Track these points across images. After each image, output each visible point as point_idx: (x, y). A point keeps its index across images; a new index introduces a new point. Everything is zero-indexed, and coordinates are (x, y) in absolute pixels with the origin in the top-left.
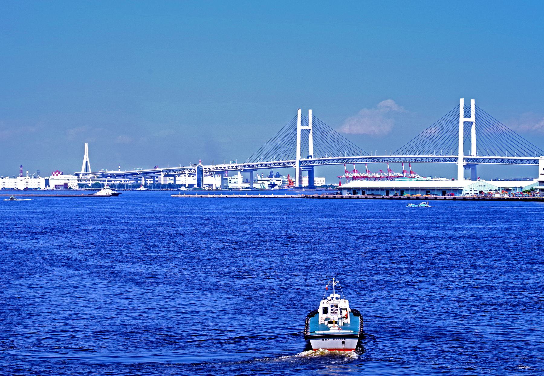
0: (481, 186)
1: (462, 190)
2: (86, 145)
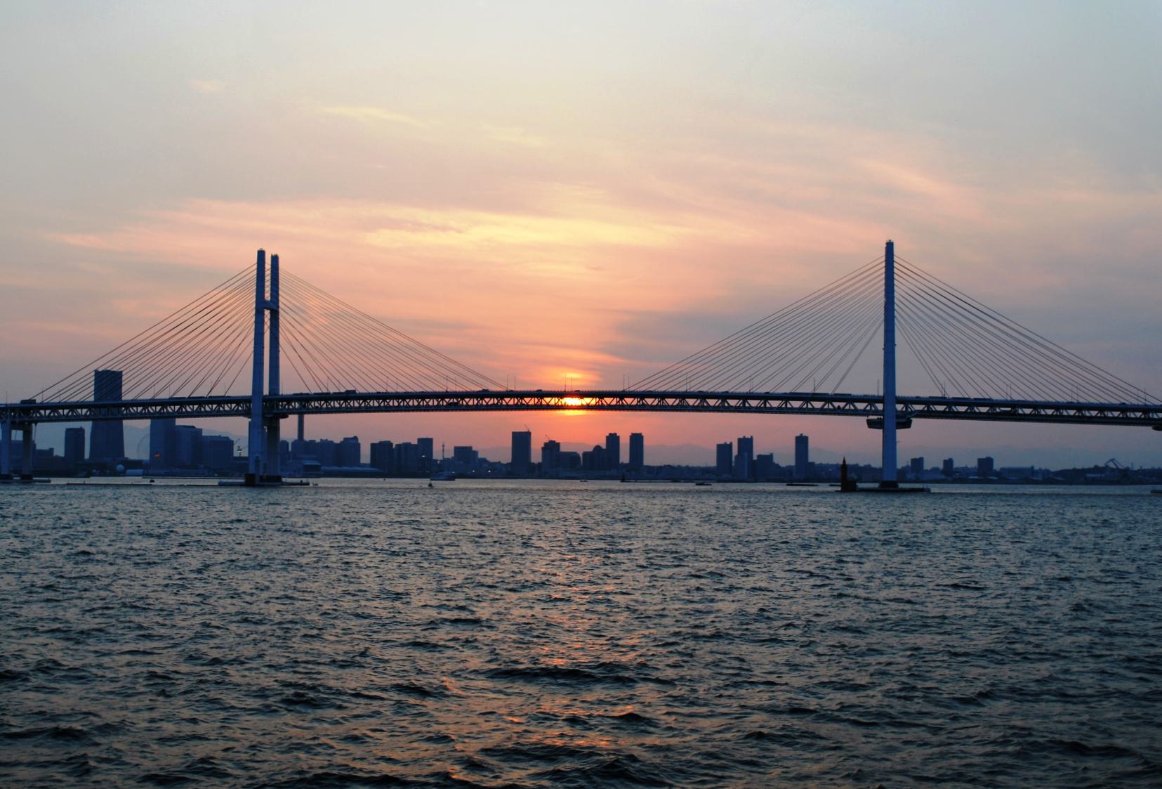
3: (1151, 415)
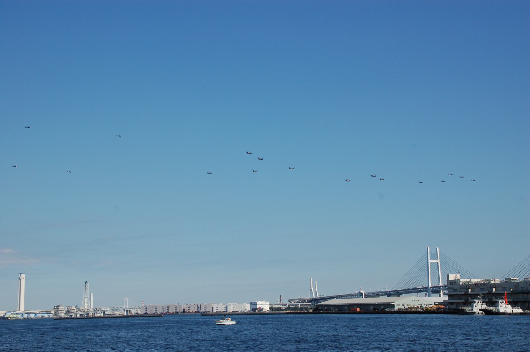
0: (414, 301)
1: (394, 305)
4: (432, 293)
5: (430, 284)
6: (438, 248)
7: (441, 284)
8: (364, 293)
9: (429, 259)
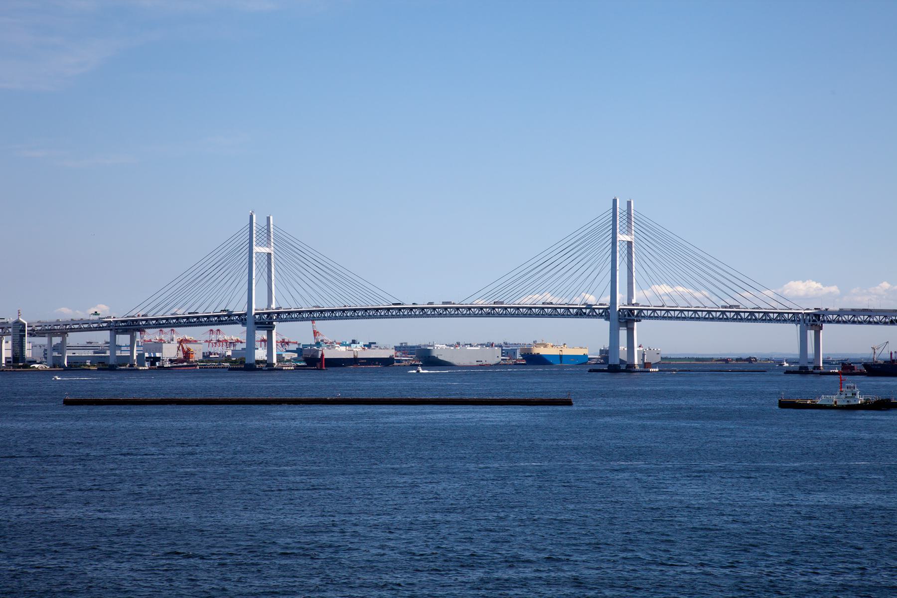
2: (66, 365)
3: (211, 320)
4: (258, 327)
5: (254, 307)
6: (271, 218)
7: (273, 306)
8: (28, 324)
9: (254, 243)
